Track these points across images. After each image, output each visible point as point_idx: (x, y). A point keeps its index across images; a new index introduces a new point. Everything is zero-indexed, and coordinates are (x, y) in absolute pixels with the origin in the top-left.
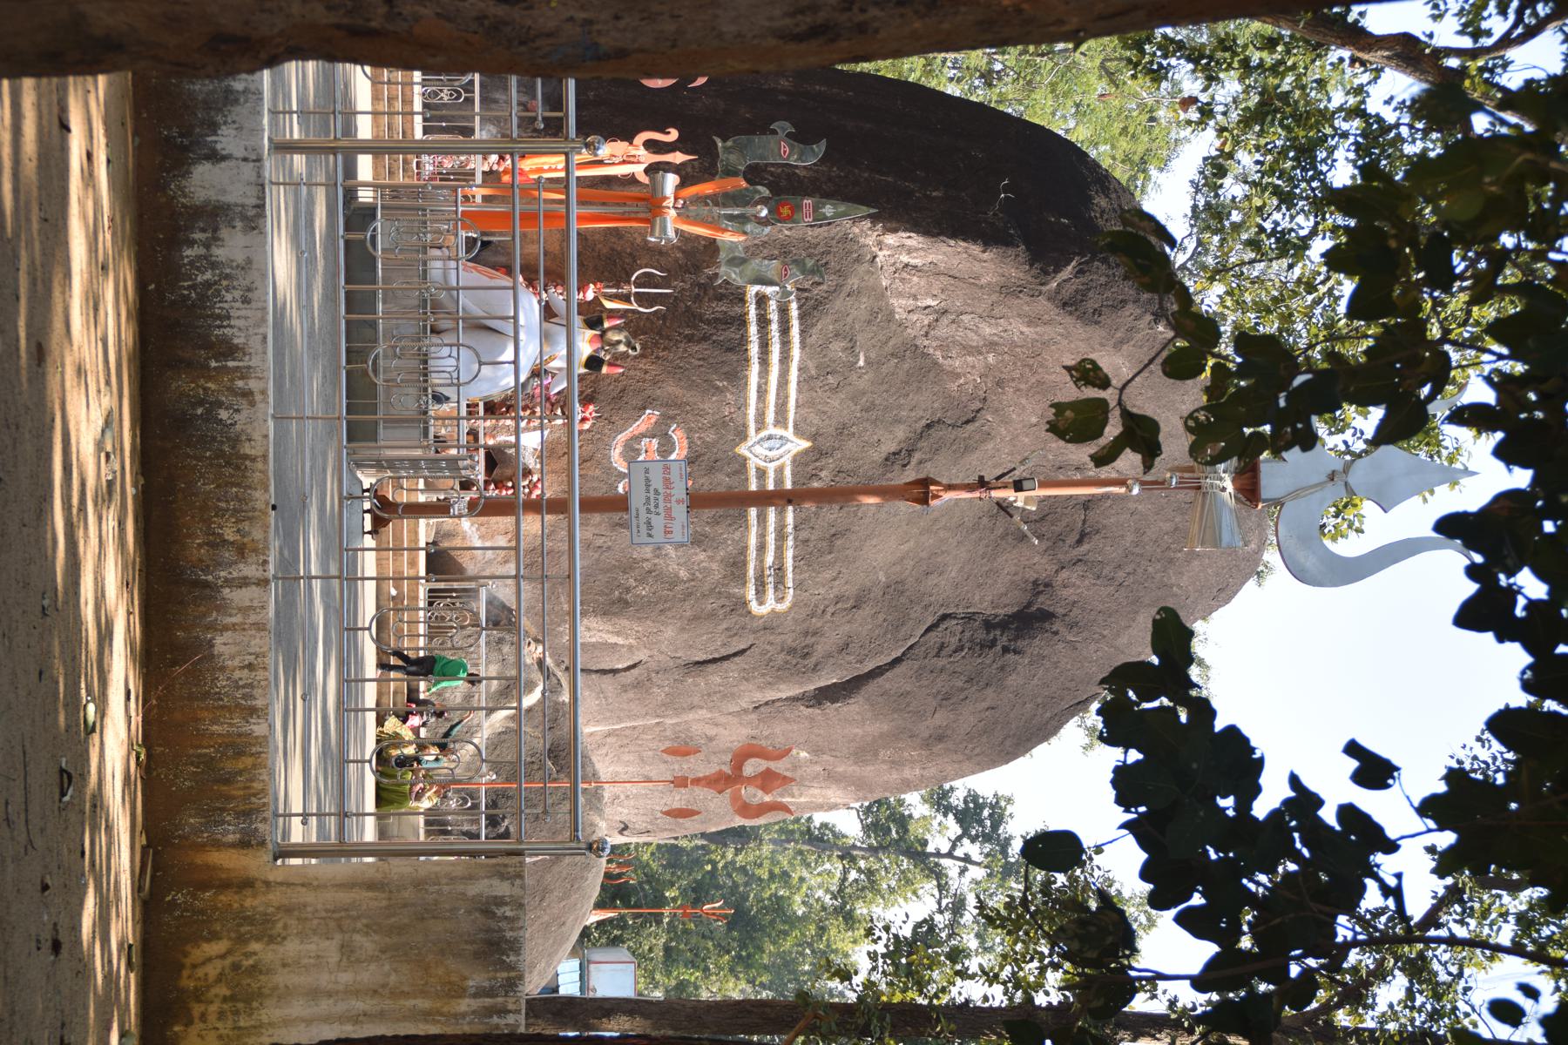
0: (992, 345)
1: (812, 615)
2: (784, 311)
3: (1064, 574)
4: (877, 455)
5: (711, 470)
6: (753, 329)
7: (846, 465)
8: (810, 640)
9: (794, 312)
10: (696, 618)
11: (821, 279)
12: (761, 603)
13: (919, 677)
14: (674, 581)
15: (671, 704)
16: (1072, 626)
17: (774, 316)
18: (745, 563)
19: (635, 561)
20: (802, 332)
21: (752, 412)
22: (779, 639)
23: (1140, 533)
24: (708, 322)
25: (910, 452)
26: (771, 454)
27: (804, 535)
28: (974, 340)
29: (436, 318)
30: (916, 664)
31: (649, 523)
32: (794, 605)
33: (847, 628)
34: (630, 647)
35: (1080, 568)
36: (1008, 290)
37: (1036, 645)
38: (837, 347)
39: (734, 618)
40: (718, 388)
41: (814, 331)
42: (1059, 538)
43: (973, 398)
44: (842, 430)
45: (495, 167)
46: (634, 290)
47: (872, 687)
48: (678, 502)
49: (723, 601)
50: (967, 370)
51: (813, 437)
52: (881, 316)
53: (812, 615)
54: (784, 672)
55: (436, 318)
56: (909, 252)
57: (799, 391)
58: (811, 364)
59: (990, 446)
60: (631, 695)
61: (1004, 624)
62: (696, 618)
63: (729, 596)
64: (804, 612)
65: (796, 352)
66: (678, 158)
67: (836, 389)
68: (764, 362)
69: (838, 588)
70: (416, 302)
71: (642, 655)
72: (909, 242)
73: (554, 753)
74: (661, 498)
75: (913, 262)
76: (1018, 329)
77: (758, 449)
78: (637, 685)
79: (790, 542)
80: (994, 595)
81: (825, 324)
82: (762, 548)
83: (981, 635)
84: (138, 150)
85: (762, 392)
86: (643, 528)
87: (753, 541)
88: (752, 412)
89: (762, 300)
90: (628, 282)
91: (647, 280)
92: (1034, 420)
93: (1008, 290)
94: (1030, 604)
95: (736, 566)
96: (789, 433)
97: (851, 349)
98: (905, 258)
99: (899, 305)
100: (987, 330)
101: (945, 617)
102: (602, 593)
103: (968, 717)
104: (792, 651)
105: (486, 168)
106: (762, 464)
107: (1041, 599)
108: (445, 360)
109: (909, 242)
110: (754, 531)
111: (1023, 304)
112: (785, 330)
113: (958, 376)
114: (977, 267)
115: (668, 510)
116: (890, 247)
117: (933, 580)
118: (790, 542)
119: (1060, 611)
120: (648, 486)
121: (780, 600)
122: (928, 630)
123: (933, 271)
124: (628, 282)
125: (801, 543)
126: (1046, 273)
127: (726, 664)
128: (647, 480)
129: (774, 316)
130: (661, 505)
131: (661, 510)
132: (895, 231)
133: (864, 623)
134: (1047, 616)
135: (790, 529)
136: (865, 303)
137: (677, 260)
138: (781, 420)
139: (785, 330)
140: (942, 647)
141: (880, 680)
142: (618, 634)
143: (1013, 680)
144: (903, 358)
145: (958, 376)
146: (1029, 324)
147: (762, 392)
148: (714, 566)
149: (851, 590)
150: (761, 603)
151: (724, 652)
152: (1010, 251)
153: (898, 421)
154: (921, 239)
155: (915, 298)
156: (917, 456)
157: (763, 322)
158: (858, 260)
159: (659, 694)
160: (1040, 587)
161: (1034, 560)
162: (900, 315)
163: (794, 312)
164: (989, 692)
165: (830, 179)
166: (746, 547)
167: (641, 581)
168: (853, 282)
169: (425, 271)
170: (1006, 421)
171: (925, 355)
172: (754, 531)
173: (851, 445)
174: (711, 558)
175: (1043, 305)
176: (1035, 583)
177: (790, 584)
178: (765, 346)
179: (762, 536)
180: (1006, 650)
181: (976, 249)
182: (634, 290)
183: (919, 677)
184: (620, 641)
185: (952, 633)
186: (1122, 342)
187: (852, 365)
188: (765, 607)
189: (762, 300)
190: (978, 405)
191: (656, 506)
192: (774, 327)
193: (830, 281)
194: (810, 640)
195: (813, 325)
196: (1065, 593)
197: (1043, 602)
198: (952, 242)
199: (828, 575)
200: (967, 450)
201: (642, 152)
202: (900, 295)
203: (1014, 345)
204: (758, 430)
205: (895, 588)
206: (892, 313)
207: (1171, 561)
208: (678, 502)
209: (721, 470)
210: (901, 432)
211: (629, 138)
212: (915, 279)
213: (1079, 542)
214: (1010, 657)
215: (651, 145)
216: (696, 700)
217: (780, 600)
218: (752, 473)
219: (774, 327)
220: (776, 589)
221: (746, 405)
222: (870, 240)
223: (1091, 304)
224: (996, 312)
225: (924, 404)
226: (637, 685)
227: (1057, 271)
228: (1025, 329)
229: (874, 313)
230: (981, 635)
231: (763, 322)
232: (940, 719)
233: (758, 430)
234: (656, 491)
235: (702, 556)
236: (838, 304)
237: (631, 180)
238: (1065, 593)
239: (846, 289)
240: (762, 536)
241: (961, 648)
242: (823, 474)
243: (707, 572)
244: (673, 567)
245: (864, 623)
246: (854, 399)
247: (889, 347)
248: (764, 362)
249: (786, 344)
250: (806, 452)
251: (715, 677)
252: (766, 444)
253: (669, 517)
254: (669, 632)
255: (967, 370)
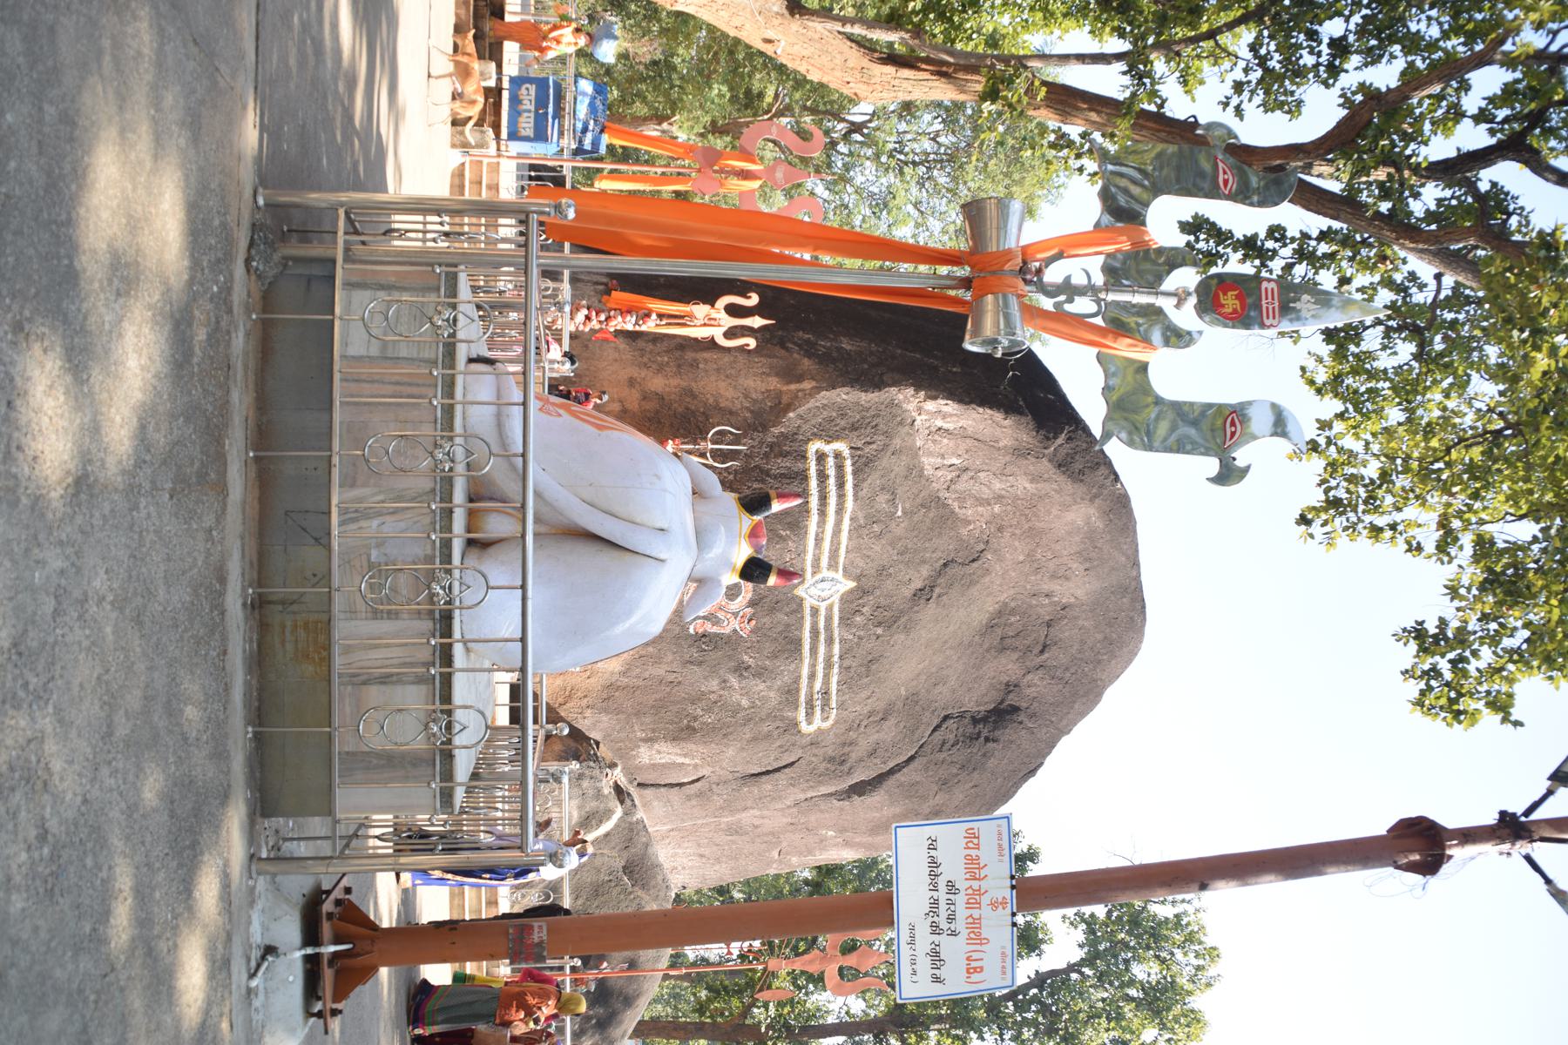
0: (999, 498)
1: (849, 730)
2: (840, 468)
3: (1029, 677)
4: (907, 592)
5: (772, 610)
6: (813, 483)
7: (883, 601)
8: (847, 749)
9: (849, 469)
10: (754, 739)
11: (873, 442)
12: (809, 723)
13: (927, 769)
14: (737, 709)
15: (728, 807)
16: (1032, 716)
17: (831, 472)
18: (798, 690)
19: (703, 694)
20: (855, 486)
21: (809, 558)
22: (820, 752)
23: (1083, 642)
24: (775, 477)
25: (932, 588)
26: (824, 595)
27: (847, 663)
28: (986, 493)
29: (481, 513)
30: (924, 760)
31: (936, 956)
32: (836, 722)
33: (876, 736)
34: (696, 766)
35: (1040, 672)
36: (1019, 453)
37: (1006, 734)
38: (882, 499)
39: (787, 736)
40: (781, 537)
41: (865, 485)
42: (1029, 649)
43: (978, 540)
44: (882, 572)
45: (581, 328)
46: (710, 446)
47: (891, 782)
48: (994, 905)
49: (778, 723)
50: (975, 517)
51: (858, 578)
52: (914, 472)
53: (849, 730)
54: (820, 777)
55: (481, 513)
56: (944, 417)
57: (850, 539)
58: (860, 515)
59: (987, 579)
60: (694, 802)
61: (984, 720)
62: (754, 739)
63: (783, 719)
64: (843, 727)
65: (850, 503)
66: (757, 322)
67: (879, 536)
68: (822, 513)
69: (872, 704)
70: (427, 484)
71: (706, 771)
72: (945, 409)
73: (628, 869)
74: (960, 899)
75: (946, 426)
76: (1023, 485)
77: (813, 591)
78: (700, 795)
79: (836, 670)
80: (977, 699)
81: (874, 479)
82: (812, 676)
83: (970, 730)
84: (69, 222)
85: (819, 540)
86: (924, 964)
87: (805, 672)
88: (809, 558)
89: (821, 457)
90: (705, 439)
91: (720, 437)
92: (1021, 558)
93: (1019, 453)
94: (1002, 702)
95: (791, 693)
96: (839, 575)
97: (892, 502)
98: (939, 423)
99: (928, 463)
100: (998, 485)
101: (946, 718)
102: (671, 722)
103: (959, 795)
104: (831, 760)
105: (573, 328)
106: (815, 603)
107: (1011, 696)
108: (491, 610)
109: (945, 409)
110: (807, 661)
111: (1030, 465)
112: (841, 485)
113: (969, 523)
114: (998, 432)
115: (975, 924)
116: (928, 413)
117: (939, 688)
118: (836, 670)
119: (1024, 705)
120: (934, 875)
121: (825, 719)
122: (934, 730)
123: (963, 434)
124: (705, 439)
125: (845, 669)
126: (1048, 439)
127: (777, 775)
128: (934, 863)
129: (831, 472)
130: (962, 912)
131: (960, 925)
132: (935, 398)
133: (888, 732)
134: (1015, 709)
135: (836, 658)
136: (904, 460)
137: (745, 420)
138: (833, 565)
139: (841, 485)
140: (944, 743)
141: (898, 776)
142: (685, 756)
143: (992, 763)
144: (929, 509)
145: (969, 523)
146: (1032, 481)
147: (819, 540)
148: (772, 694)
149: (881, 705)
150: (809, 723)
151: (776, 765)
152: (1023, 419)
153: (924, 562)
154: (956, 406)
155: (943, 457)
156: (937, 590)
157: (822, 477)
158: (901, 423)
159: (718, 801)
160: (1011, 687)
161: (1007, 667)
162: (929, 471)
163: (849, 469)
164: (976, 775)
165: (872, 353)
166: (799, 677)
167: (709, 710)
168: (897, 442)
169: (449, 411)
170: (1000, 560)
171: (946, 506)
172: (807, 661)
173: (889, 584)
174: (769, 688)
175: (1045, 466)
176: (1007, 685)
177: (834, 705)
178: (823, 498)
179: (813, 666)
180: (987, 740)
181: (998, 416)
182: (710, 446)
183: (927, 769)
184: (687, 761)
185: (950, 732)
186: (1095, 496)
187: (892, 516)
188: (811, 726)
189: (821, 457)
190: (982, 546)
191: (951, 918)
192: (832, 481)
193: (880, 440)
194: (847, 749)
195: (864, 480)
196: (1028, 691)
197: (1012, 699)
198: (981, 410)
199: (865, 694)
200: (972, 583)
201: (723, 315)
202: (930, 454)
203: (1016, 498)
204: (814, 573)
205: (912, 699)
206: (922, 470)
207: (1099, 662)
208: (994, 905)
209: (780, 610)
210: (925, 571)
211: (711, 302)
212: (945, 441)
213: (1042, 652)
214: (990, 745)
215: (732, 310)
216: (749, 803)
217: (825, 719)
218: (807, 612)
219: (832, 481)
220: (823, 710)
221: (804, 551)
222: (911, 407)
223: (1078, 466)
224: (1007, 471)
225: (943, 546)
226: (700, 795)
227: (1055, 438)
228: (1028, 485)
229: (910, 470)
230: (970, 730)
231: (822, 477)
232: (939, 799)
233: (814, 573)
234: (951, 887)
235: (762, 686)
236: (885, 461)
237: (711, 344)
238: (1028, 691)
239: (891, 449)
240: (813, 666)
241: (956, 743)
242: (864, 610)
243: (765, 699)
244: (736, 697)
245: (888, 732)
246: (892, 544)
247: (919, 501)
248: (822, 513)
249: (841, 496)
250: (851, 591)
251: (767, 785)
252: (820, 586)
253: (977, 938)
254: (731, 752)
255: (975, 517)
